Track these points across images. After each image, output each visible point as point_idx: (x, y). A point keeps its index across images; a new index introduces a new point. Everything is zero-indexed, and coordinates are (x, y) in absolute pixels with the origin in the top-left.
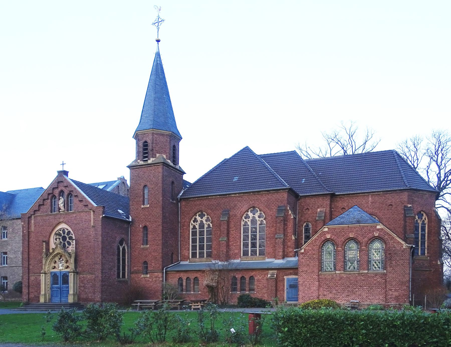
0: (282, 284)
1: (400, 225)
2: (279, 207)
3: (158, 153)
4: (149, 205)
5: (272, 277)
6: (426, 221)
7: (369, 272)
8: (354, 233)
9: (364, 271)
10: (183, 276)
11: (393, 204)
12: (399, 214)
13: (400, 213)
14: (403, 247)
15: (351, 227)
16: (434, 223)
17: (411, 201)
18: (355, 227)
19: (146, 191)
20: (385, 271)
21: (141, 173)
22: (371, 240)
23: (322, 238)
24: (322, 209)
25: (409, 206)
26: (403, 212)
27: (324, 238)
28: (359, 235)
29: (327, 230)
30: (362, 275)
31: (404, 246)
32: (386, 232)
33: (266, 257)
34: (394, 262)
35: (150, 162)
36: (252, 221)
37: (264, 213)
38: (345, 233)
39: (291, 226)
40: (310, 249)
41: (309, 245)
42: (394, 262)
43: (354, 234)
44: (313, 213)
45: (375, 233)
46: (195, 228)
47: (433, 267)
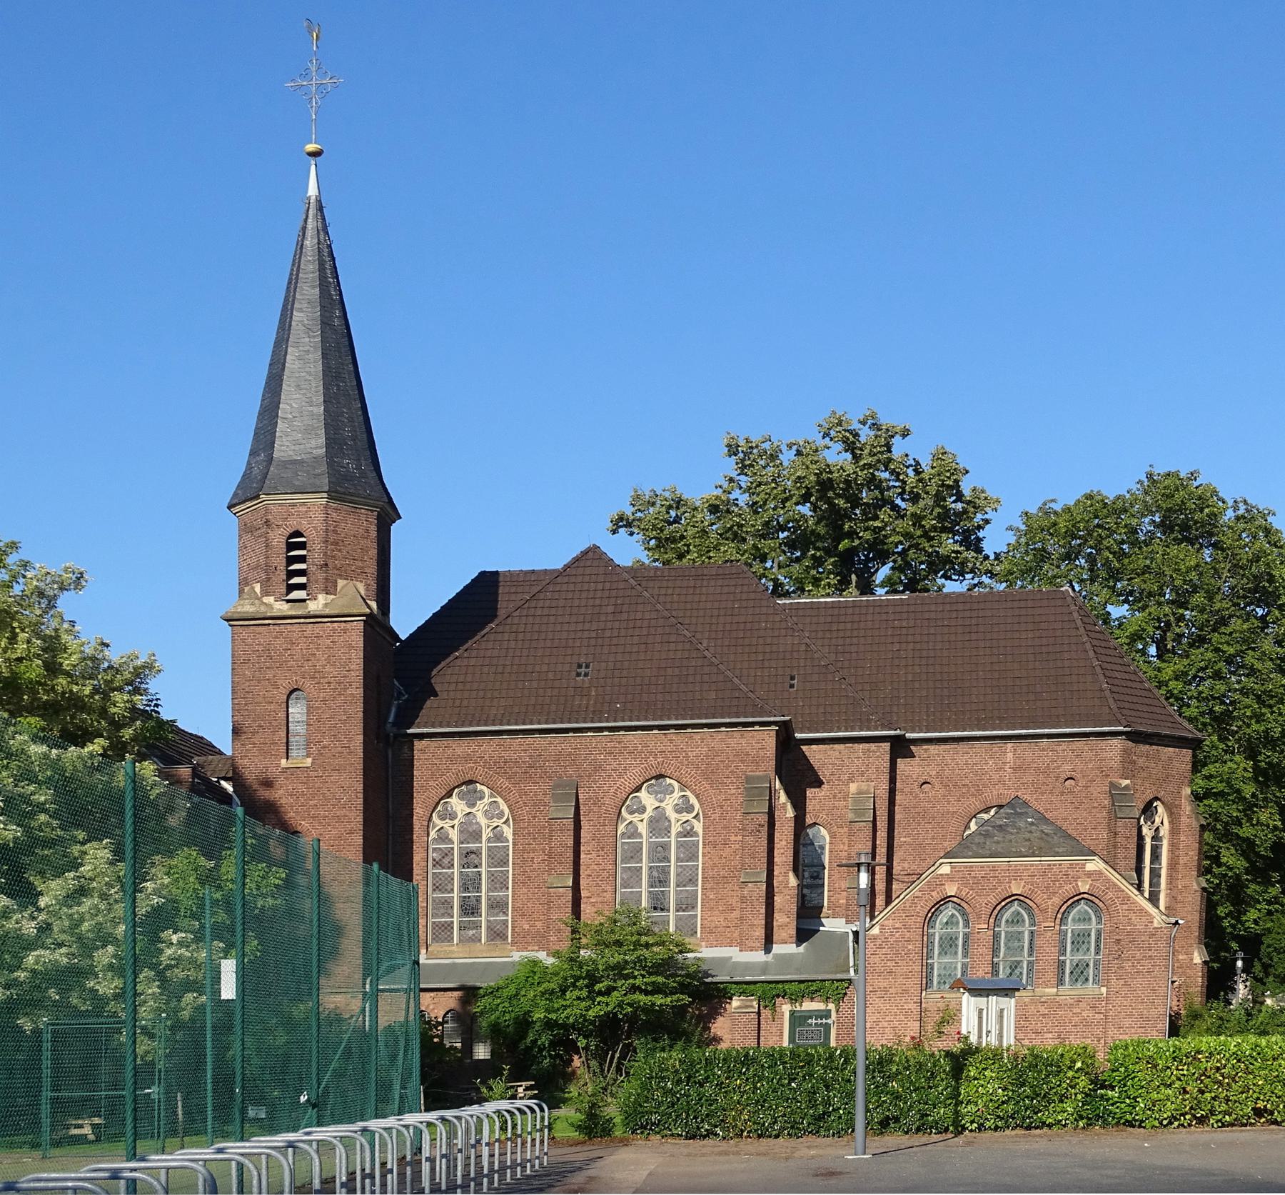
0: (774, 1030)
1: (1097, 842)
2: (749, 779)
3: (341, 576)
4: (309, 760)
5: (747, 1007)
6: (1165, 831)
7: (1060, 993)
8: (1023, 883)
9: (1047, 990)
10: (431, 1007)
11: (1079, 776)
12: (1094, 807)
13: (1096, 805)
14: (1152, 922)
15: (1016, 866)
16: (1187, 836)
17: (1129, 768)
18: (1026, 866)
19: (297, 711)
20: (1104, 990)
21: (280, 644)
22: (1069, 903)
23: (933, 894)
24: (864, 786)
25: (1126, 782)
26: (1106, 802)
27: (938, 893)
28: (1037, 887)
29: (949, 872)
30: (1042, 1000)
31: (1155, 921)
32: (1109, 881)
33: (703, 944)
34: (1127, 965)
35: (313, 607)
36: (652, 821)
37: (697, 796)
38: (1000, 883)
39: (784, 843)
40: (897, 926)
41: (894, 913)
42: (1127, 965)
43: (1024, 886)
44: (835, 797)
45: (1080, 884)
46: (447, 837)
47: (1180, 970)
